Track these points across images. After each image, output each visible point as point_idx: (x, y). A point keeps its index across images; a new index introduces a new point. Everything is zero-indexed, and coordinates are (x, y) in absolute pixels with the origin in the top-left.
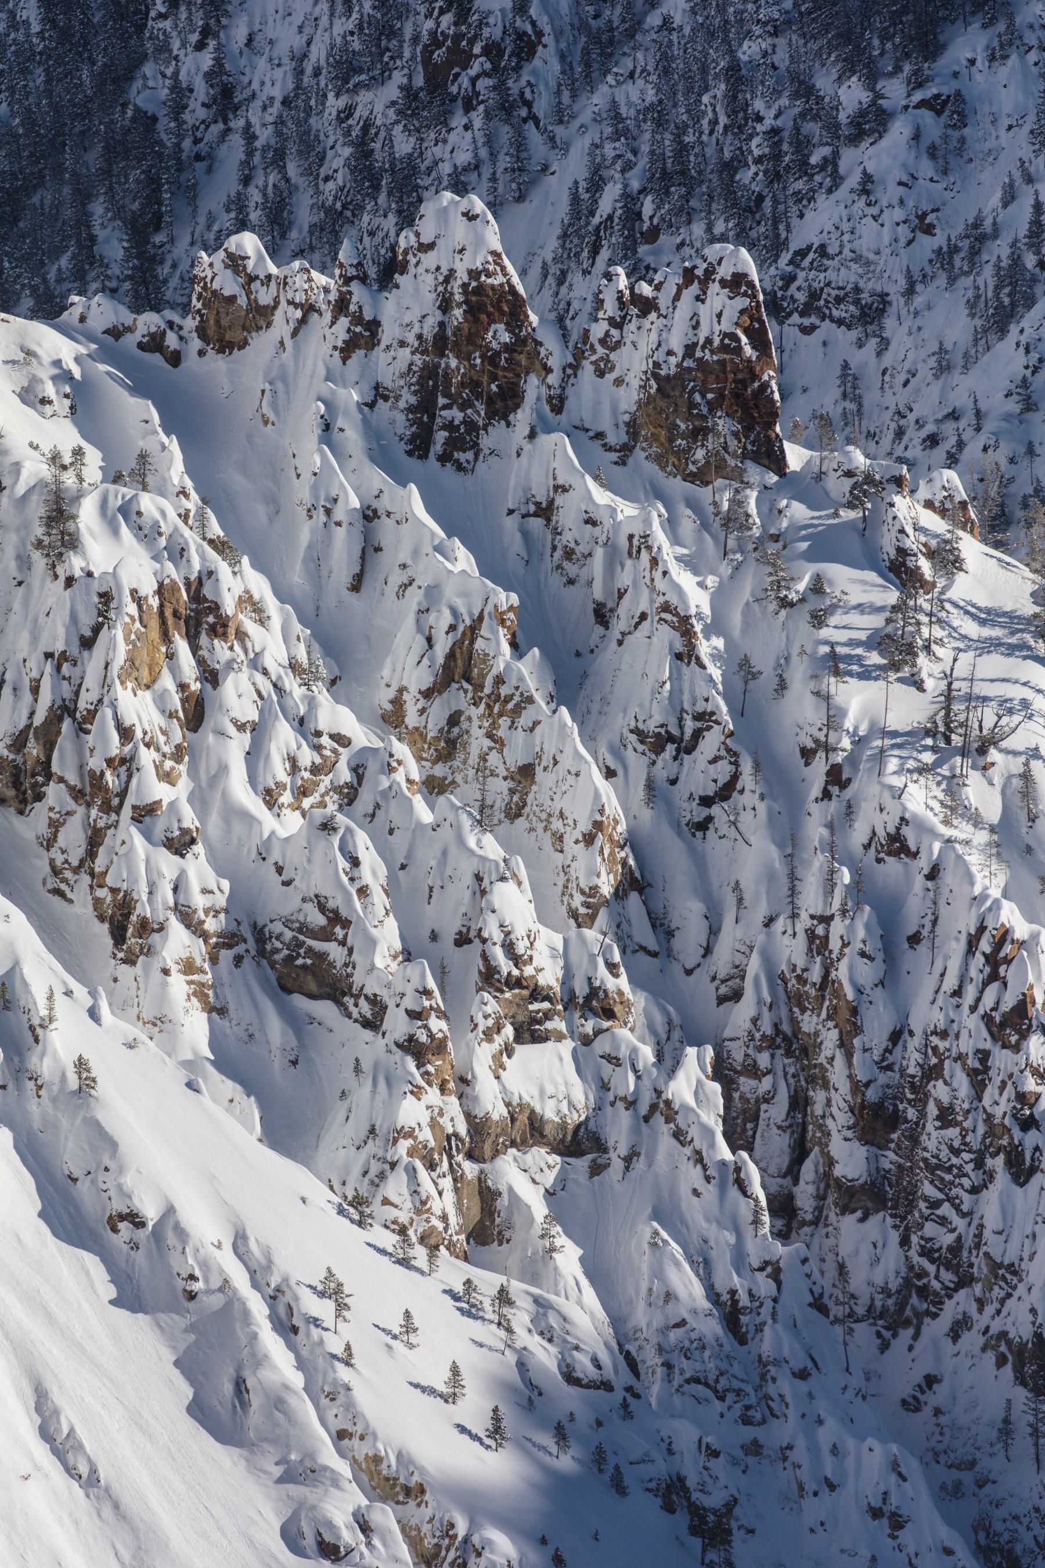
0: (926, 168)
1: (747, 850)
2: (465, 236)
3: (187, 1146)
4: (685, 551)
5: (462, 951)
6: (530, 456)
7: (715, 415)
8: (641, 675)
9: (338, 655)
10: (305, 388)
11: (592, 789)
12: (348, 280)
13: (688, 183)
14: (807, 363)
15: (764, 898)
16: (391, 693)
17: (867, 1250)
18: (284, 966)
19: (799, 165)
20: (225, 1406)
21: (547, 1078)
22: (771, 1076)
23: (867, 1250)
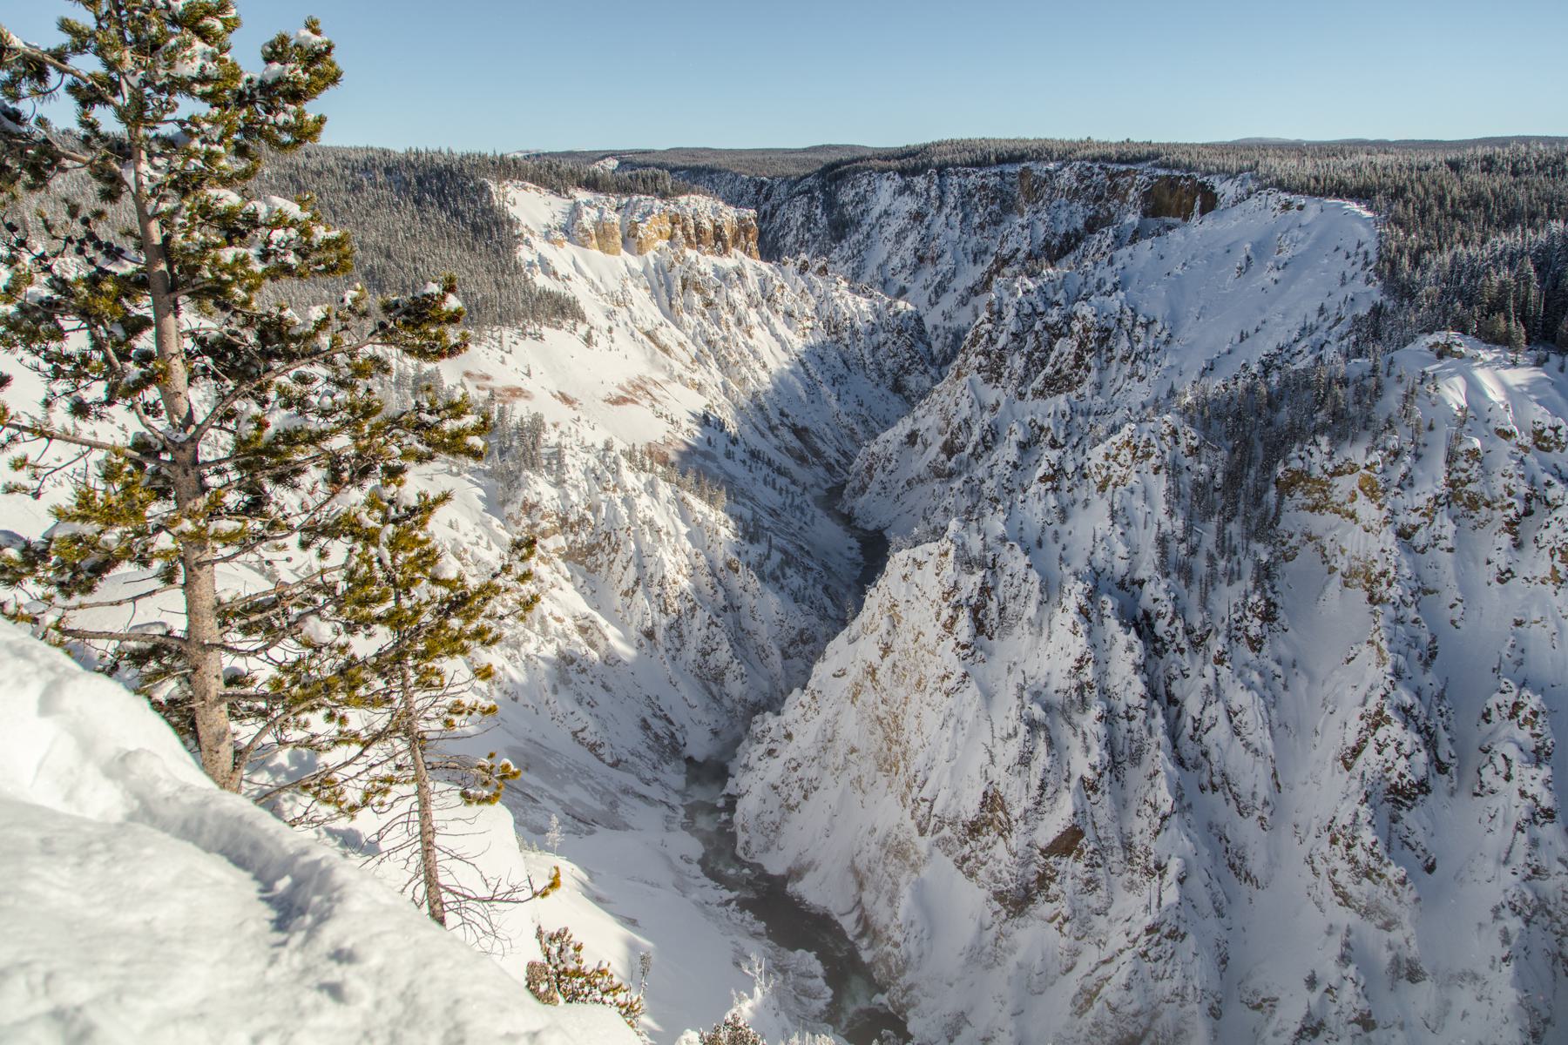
0: (1188, 816)
1: (825, 306)
2: (803, 257)
3: (781, 329)
4: (1198, 203)
5: (803, 314)
6: (809, 274)
7: (823, 271)
8: (817, 292)
9: (794, 290)
10: (791, 268)
11: (813, 301)
12: (1042, 314)
13: (823, 252)
14: (830, 267)
15: (826, 310)
16: (516, 380)
17: (834, 337)
18: (789, 314)
19: (830, 251)
20: (784, 349)
21: (809, 324)
22: (827, 324)
23: (834, 337)
